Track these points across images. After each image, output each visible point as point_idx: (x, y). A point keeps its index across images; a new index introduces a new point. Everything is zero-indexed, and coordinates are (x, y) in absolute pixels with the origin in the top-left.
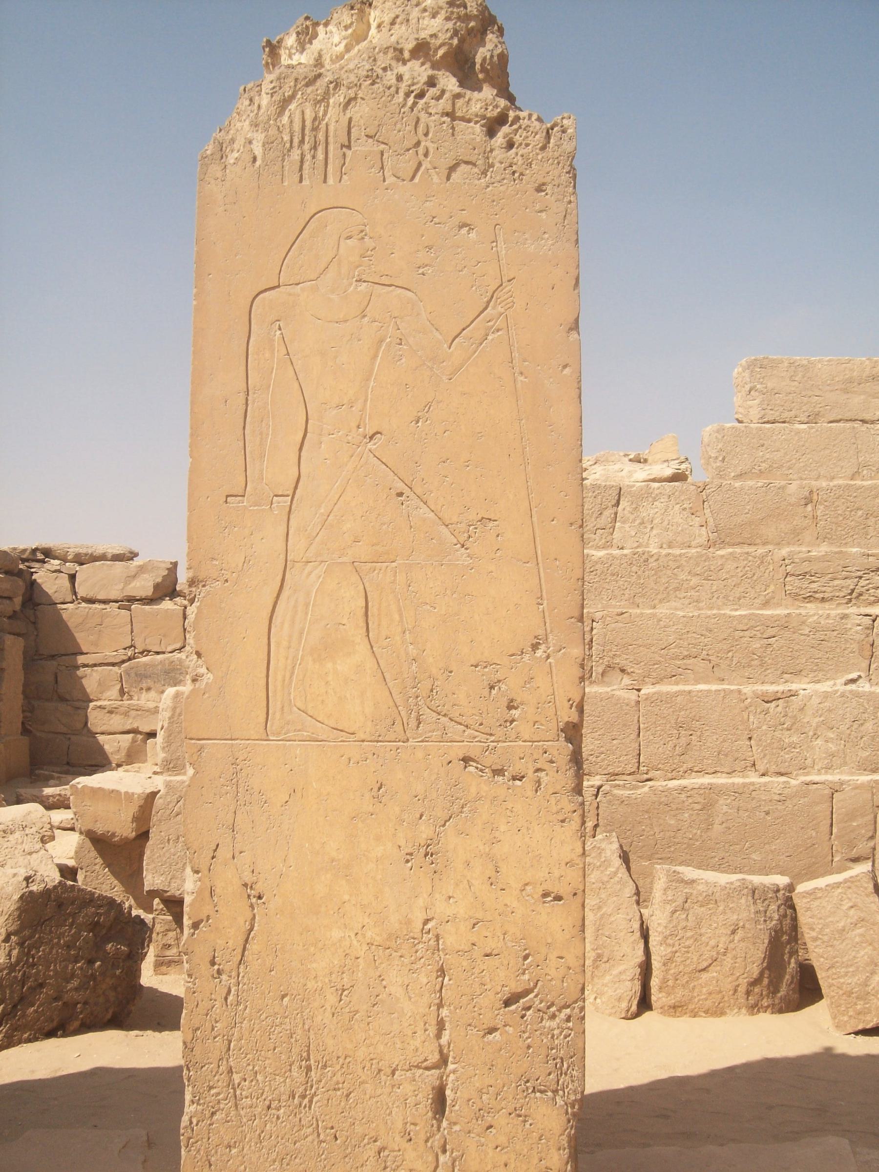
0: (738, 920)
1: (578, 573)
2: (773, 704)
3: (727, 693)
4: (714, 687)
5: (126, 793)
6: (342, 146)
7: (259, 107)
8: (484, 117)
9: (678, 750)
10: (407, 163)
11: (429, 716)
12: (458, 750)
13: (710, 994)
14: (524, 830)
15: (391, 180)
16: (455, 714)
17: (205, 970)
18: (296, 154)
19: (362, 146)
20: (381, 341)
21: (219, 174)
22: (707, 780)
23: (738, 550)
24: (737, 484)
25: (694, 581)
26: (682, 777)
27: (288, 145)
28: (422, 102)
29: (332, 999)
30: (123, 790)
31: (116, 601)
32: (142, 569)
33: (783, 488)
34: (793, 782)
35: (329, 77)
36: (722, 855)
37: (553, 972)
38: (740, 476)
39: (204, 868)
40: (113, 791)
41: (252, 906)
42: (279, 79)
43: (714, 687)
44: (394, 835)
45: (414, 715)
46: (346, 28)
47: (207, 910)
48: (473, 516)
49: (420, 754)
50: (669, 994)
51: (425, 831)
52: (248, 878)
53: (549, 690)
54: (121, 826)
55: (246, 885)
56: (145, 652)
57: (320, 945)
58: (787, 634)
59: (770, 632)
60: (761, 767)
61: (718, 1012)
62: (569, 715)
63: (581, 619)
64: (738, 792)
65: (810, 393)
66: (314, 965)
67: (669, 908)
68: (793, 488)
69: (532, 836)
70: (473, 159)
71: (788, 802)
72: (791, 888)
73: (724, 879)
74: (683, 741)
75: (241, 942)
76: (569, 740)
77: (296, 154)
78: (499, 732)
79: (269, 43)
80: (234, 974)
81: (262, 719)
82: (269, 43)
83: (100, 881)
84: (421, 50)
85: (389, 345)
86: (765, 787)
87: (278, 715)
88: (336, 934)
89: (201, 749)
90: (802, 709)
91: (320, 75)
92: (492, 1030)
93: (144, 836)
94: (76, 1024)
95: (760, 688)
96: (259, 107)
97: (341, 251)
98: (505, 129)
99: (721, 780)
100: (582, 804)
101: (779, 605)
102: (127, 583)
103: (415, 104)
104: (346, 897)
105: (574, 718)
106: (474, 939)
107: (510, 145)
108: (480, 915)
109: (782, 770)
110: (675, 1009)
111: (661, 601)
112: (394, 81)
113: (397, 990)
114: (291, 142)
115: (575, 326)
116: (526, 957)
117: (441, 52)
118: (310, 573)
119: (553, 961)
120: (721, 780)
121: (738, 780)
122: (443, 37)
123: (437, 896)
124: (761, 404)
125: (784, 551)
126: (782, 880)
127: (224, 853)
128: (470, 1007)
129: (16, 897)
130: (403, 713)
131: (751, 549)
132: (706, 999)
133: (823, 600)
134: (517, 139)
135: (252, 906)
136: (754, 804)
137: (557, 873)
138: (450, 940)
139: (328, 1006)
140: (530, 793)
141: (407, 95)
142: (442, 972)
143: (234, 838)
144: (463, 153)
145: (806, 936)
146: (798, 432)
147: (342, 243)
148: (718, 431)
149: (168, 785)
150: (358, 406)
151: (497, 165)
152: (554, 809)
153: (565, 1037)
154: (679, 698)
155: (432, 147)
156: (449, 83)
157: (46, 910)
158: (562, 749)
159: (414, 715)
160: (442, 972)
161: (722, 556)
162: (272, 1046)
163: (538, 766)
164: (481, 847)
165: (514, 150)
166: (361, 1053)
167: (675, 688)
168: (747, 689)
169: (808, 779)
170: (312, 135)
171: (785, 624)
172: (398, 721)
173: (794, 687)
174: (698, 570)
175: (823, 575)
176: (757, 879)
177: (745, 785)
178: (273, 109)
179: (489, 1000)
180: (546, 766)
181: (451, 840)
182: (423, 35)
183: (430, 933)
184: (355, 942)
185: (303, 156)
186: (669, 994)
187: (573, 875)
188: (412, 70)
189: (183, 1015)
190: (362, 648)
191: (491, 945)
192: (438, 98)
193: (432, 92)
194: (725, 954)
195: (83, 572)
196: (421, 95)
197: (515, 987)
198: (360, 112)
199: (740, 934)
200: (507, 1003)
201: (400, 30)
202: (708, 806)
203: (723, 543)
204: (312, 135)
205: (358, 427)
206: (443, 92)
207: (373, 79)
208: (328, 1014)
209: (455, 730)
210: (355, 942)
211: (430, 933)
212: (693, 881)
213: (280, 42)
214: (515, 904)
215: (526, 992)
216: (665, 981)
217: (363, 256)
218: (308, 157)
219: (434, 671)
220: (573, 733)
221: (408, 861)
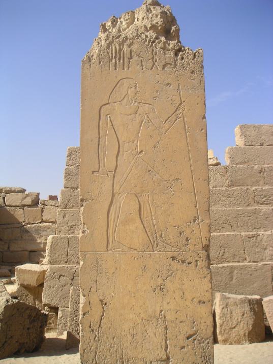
0: (244, 311)
1: (208, 196)
2: (252, 238)
3: (236, 236)
4: (232, 233)
5: (34, 271)
6: (129, 58)
7: (101, 45)
8: (174, 49)
9: (221, 254)
10: (150, 63)
11: (161, 243)
12: (170, 255)
13: (236, 336)
14: (192, 280)
15: (144, 69)
16: (169, 243)
17: (87, 329)
18: (113, 61)
19: (135, 59)
20: (142, 121)
21: (88, 67)
22: (230, 264)
23: (239, 188)
24: (238, 166)
25: (224, 198)
26: (222, 263)
27: (111, 58)
28: (154, 44)
29: (130, 338)
30: (33, 270)
31: (19, 206)
32: (28, 195)
33: (253, 167)
34: (259, 264)
35: (123, 36)
36: (236, 289)
37: (203, 327)
38: (239, 163)
39: (86, 294)
40: (29, 270)
41: (103, 308)
42: (107, 36)
43: (232, 233)
44: (150, 283)
45: (155, 243)
46: (127, 20)
47: (88, 309)
48: (173, 178)
49: (158, 256)
50: (222, 336)
51: (160, 281)
52: (101, 298)
53: (199, 233)
54: (33, 282)
55: (101, 301)
56: (29, 223)
57: (126, 320)
58: (256, 215)
59: (250, 215)
60: (248, 260)
61: (238, 342)
62: (205, 242)
63: (209, 210)
64: (241, 268)
65: (260, 136)
66: (124, 327)
67: (221, 307)
68: (256, 167)
69: (195, 282)
70: (171, 63)
71: (258, 272)
72: (261, 300)
73: (239, 297)
74: (222, 251)
75: (100, 318)
76: (206, 251)
77: (113, 61)
78: (183, 248)
79: (102, 25)
80: (97, 330)
81: (105, 245)
82: (102, 25)
83: (29, 300)
84: (153, 27)
85: (145, 122)
86: (250, 267)
87: (111, 244)
88: (131, 316)
89: (85, 255)
90: (261, 240)
91: (120, 35)
92: (183, 347)
93: (42, 285)
94: (23, 350)
95: (247, 233)
96: (101, 45)
97: (129, 92)
98: (181, 53)
99: (235, 264)
100: (211, 271)
101: (252, 206)
102: (22, 200)
103: (152, 45)
104: (134, 304)
105: (208, 243)
106: (177, 317)
107: (182, 58)
108: (178, 309)
109: (255, 260)
110: (225, 341)
111: (214, 205)
112: (144, 37)
113: (152, 335)
114: (112, 57)
115: (204, 117)
116: (194, 323)
117: (159, 28)
118: (120, 197)
119: (202, 324)
120: (235, 264)
121: (241, 264)
122: (160, 23)
123: (164, 302)
124: (245, 140)
125: (254, 188)
126: (258, 297)
127: (93, 290)
128: (176, 340)
129: (3, 307)
130: (152, 242)
131: (243, 188)
132: (234, 338)
133: (267, 204)
134: (185, 56)
135: (103, 308)
136: (247, 272)
137: (203, 294)
138: (168, 317)
139: (128, 340)
140: (194, 268)
141: (149, 42)
142: (166, 329)
143: (97, 285)
144: (168, 61)
145: (267, 316)
146: (258, 149)
147: (129, 89)
148: (231, 148)
149: (51, 268)
150: (135, 143)
151: (178, 65)
152: (202, 273)
153: (207, 349)
154: (221, 237)
155: (158, 59)
156: (163, 39)
157: (15, 310)
158: (203, 254)
159: (155, 243)
160: (166, 329)
161: (233, 190)
162: (110, 354)
163: (196, 259)
164: (178, 286)
165: (184, 60)
166: (140, 356)
167: (219, 234)
168: (242, 234)
169: (264, 263)
170: (119, 54)
171: (255, 212)
172: (150, 245)
173: (258, 233)
174: (226, 195)
175: (267, 196)
176: (249, 297)
177: (243, 266)
178: (105, 46)
179: (182, 337)
180: (199, 259)
181: (168, 284)
182: (154, 23)
183: (161, 316)
184: (137, 319)
185: (116, 61)
186: (222, 336)
187: (208, 295)
188: (150, 34)
189: (80, 345)
190: (138, 220)
191: (183, 318)
192: (159, 43)
193: (157, 41)
194: (241, 322)
195: (8, 197)
196: (154, 42)
197: (190, 332)
198: (135, 47)
199: (245, 315)
200: (188, 338)
201: (145, 21)
202: (231, 273)
203: (234, 186)
204: (119, 54)
205: (135, 149)
206: (161, 41)
207: (138, 36)
208: (129, 343)
209: (169, 248)
210: (137, 319)
211: (161, 316)
212: (229, 298)
213: (105, 24)
214: (190, 304)
215: (194, 334)
216: (221, 332)
217: (135, 94)
218: (117, 62)
219: (162, 228)
220: (207, 248)
221: (154, 291)
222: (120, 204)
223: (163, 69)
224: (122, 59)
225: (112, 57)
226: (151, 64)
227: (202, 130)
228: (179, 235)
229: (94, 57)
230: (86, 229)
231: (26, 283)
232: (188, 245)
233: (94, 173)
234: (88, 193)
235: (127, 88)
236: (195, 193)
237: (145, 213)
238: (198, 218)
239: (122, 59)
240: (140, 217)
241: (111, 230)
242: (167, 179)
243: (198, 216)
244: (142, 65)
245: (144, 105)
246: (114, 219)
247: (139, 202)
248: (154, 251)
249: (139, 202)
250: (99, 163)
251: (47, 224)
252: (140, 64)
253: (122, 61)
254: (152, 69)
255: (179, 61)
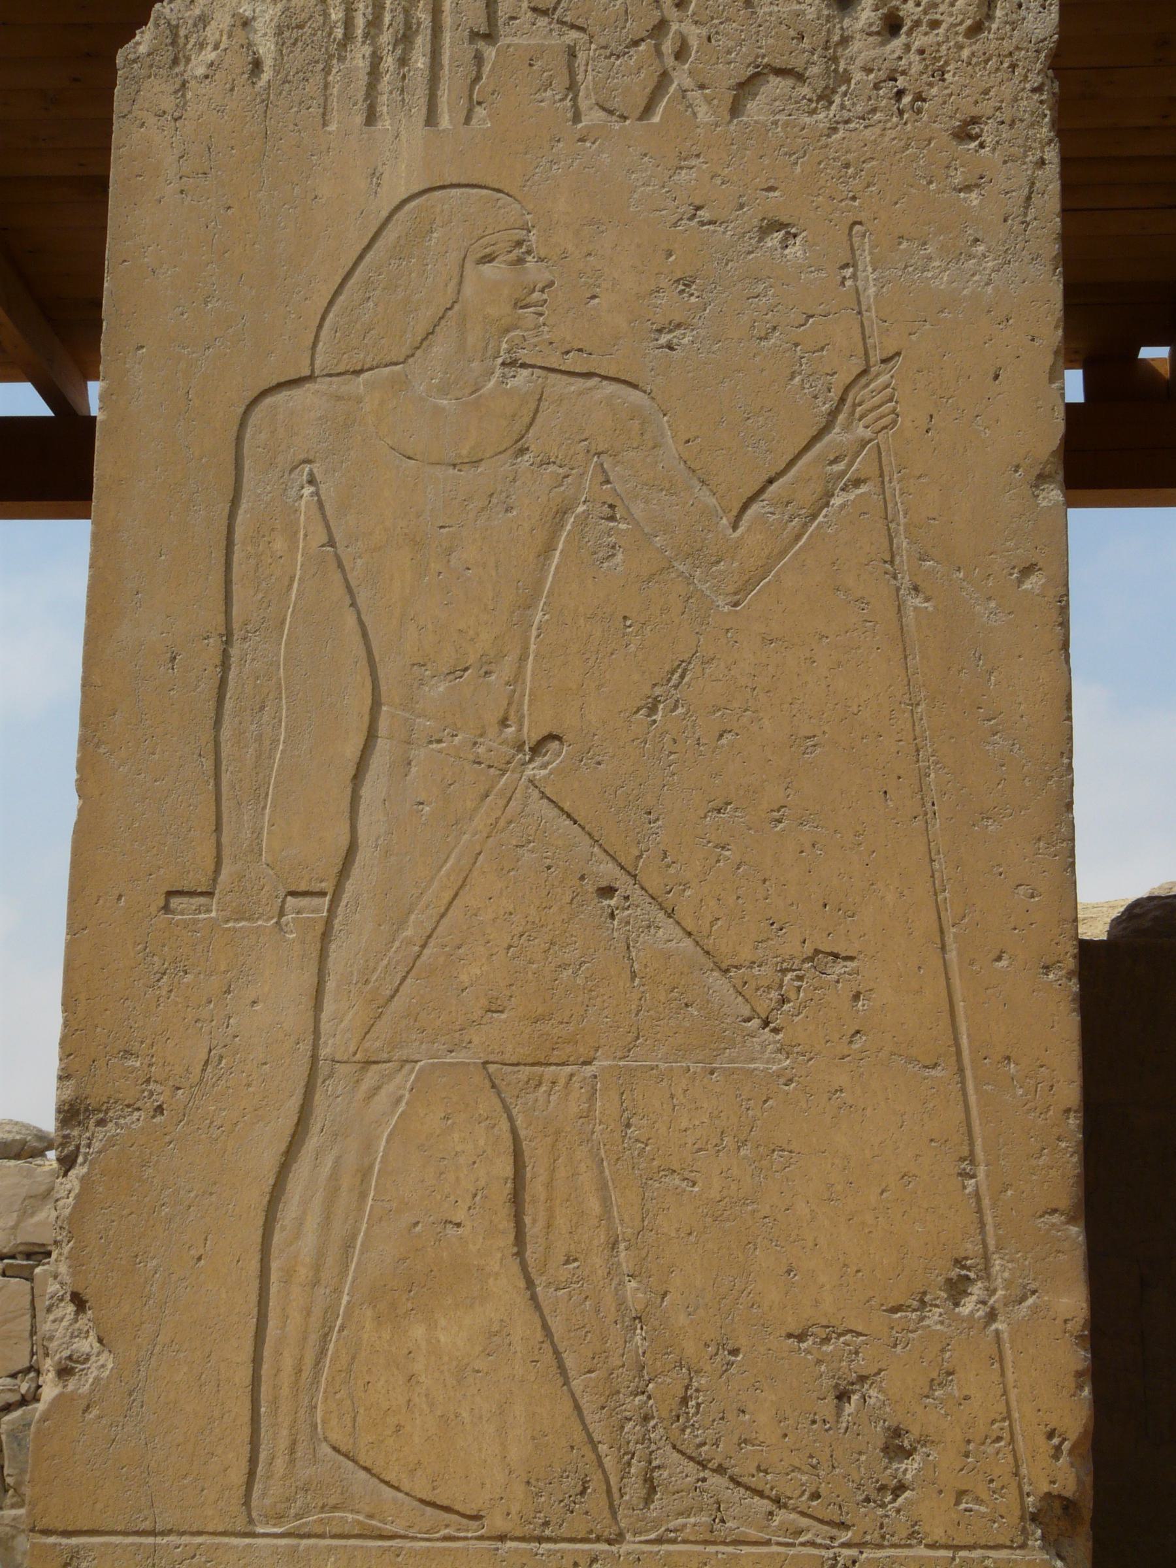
10: (632, 75)
11: (677, 1471)
15: (592, 117)
16: (744, 1467)
18: (359, 56)
20: (563, 512)
21: (168, 103)
27: (339, 33)
48: (791, 946)
70: (797, 63)
77: (359, 56)
78: (864, 1519)
81: (237, 1476)
87: (280, 1464)
97: (468, 290)
114: (348, 23)
144: (772, 49)
151: (858, 76)
185: (376, 60)
190: (505, 1284)
205: (504, 723)
217: (520, 304)
218: (389, 62)
219: (690, 1348)
222: (368, 1147)
223: (735, 110)
224: (422, 42)
225: (348, 23)
226: (645, 80)
227: (1028, 571)
228: (826, 1408)
229: (211, 33)
230: (86, 1345)
231: (463, 121)
232: (900, 1488)
233: (175, 902)
234: (128, 1053)
235: (454, 257)
236: (961, 1070)
237: (562, 1222)
238: (986, 1272)
239: (422, 42)
240: (520, 1254)
241: (282, 1361)
242: (746, 954)
243: (986, 1258)
244: (573, 87)
245: (580, 383)
246: (317, 1268)
247: (514, 1132)
248: (619, 1538)
249: (514, 1132)
250: (218, 829)
251: (453, 856)
252: (561, 81)
253: (420, 62)
254: (648, 110)
255: (862, 50)
